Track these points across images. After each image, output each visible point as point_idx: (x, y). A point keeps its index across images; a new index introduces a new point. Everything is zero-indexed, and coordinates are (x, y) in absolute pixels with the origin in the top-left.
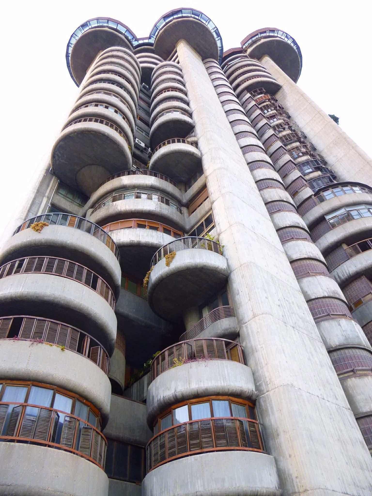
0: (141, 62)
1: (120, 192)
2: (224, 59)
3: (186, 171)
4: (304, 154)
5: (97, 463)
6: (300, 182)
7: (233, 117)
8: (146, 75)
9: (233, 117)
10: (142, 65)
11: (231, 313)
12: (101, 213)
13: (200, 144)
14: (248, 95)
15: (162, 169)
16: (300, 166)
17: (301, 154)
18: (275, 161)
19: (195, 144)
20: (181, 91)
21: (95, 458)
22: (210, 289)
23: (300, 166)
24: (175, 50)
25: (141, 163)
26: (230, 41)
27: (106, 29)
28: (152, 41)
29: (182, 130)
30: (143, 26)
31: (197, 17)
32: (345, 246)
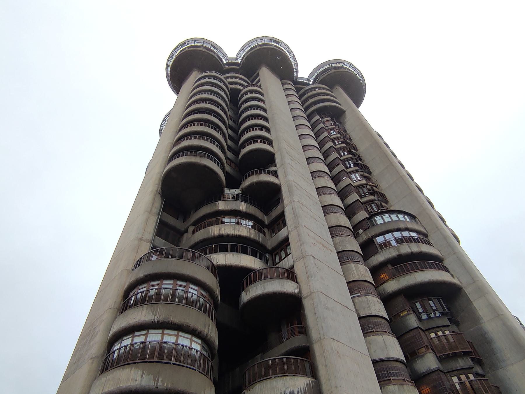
0: (231, 83)
1: (217, 216)
2: (299, 85)
3: (268, 200)
4: (342, 142)
5: (205, 374)
6: (327, 138)
7: (290, 99)
8: (234, 97)
9: (290, 99)
10: (230, 86)
11: (304, 331)
12: (200, 235)
13: (279, 173)
14: (318, 117)
15: (249, 195)
16: (338, 150)
17: (340, 143)
18: (378, 283)
19: (275, 174)
20: (257, 92)
21: (204, 370)
22: (289, 310)
23: (338, 150)
24: (256, 74)
25: (233, 183)
26: (304, 71)
27: (201, 49)
28: (239, 61)
29: (266, 160)
30: (232, 49)
31: (277, 45)
32: (390, 267)
